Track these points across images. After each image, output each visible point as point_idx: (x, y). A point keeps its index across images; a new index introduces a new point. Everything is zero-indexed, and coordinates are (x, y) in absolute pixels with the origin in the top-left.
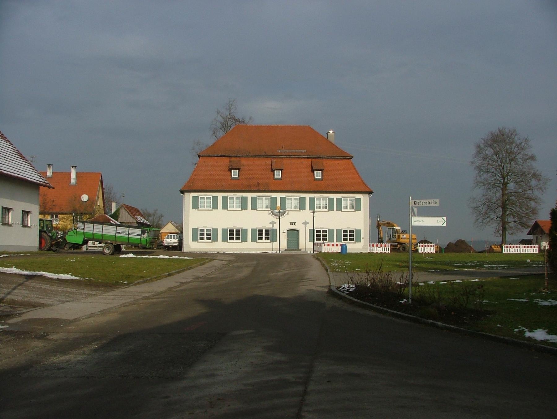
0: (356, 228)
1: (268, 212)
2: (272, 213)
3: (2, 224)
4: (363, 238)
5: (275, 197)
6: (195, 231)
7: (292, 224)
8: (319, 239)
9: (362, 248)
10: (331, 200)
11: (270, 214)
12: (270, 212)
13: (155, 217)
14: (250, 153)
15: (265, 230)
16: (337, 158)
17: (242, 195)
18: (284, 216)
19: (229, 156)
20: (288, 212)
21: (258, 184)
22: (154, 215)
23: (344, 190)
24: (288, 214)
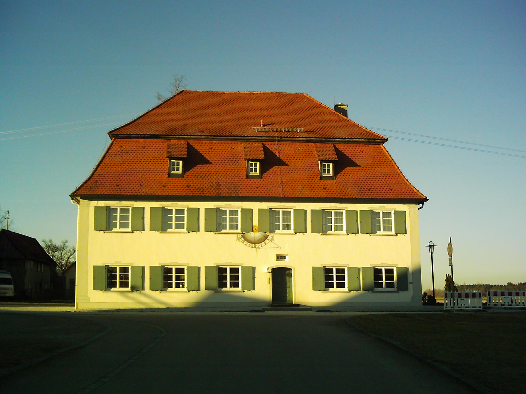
0: (243, 264)
1: (235, 236)
2: (244, 239)
3: (519, 283)
4: (411, 283)
5: (278, 211)
6: (410, 282)
7: (280, 258)
8: (236, 285)
9: (410, 301)
10: (166, 212)
11: (239, 239)
12: (240, 236)
13: (64, 252)
14: (203, 132)
15: (231, 268)
16: (358, 142)
17: (133, 204)
18: (266, 244)
19: (166, 137)
20: (273, 237)
21: (218, 185)
22: (63, 249)
23: (128, 193)
24: (272, 239)
